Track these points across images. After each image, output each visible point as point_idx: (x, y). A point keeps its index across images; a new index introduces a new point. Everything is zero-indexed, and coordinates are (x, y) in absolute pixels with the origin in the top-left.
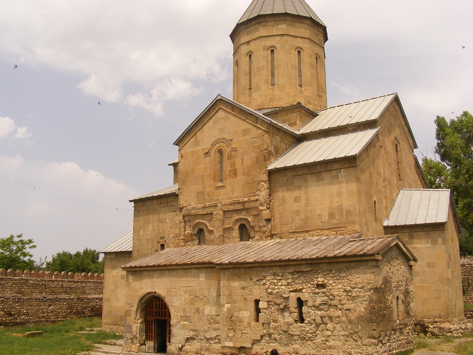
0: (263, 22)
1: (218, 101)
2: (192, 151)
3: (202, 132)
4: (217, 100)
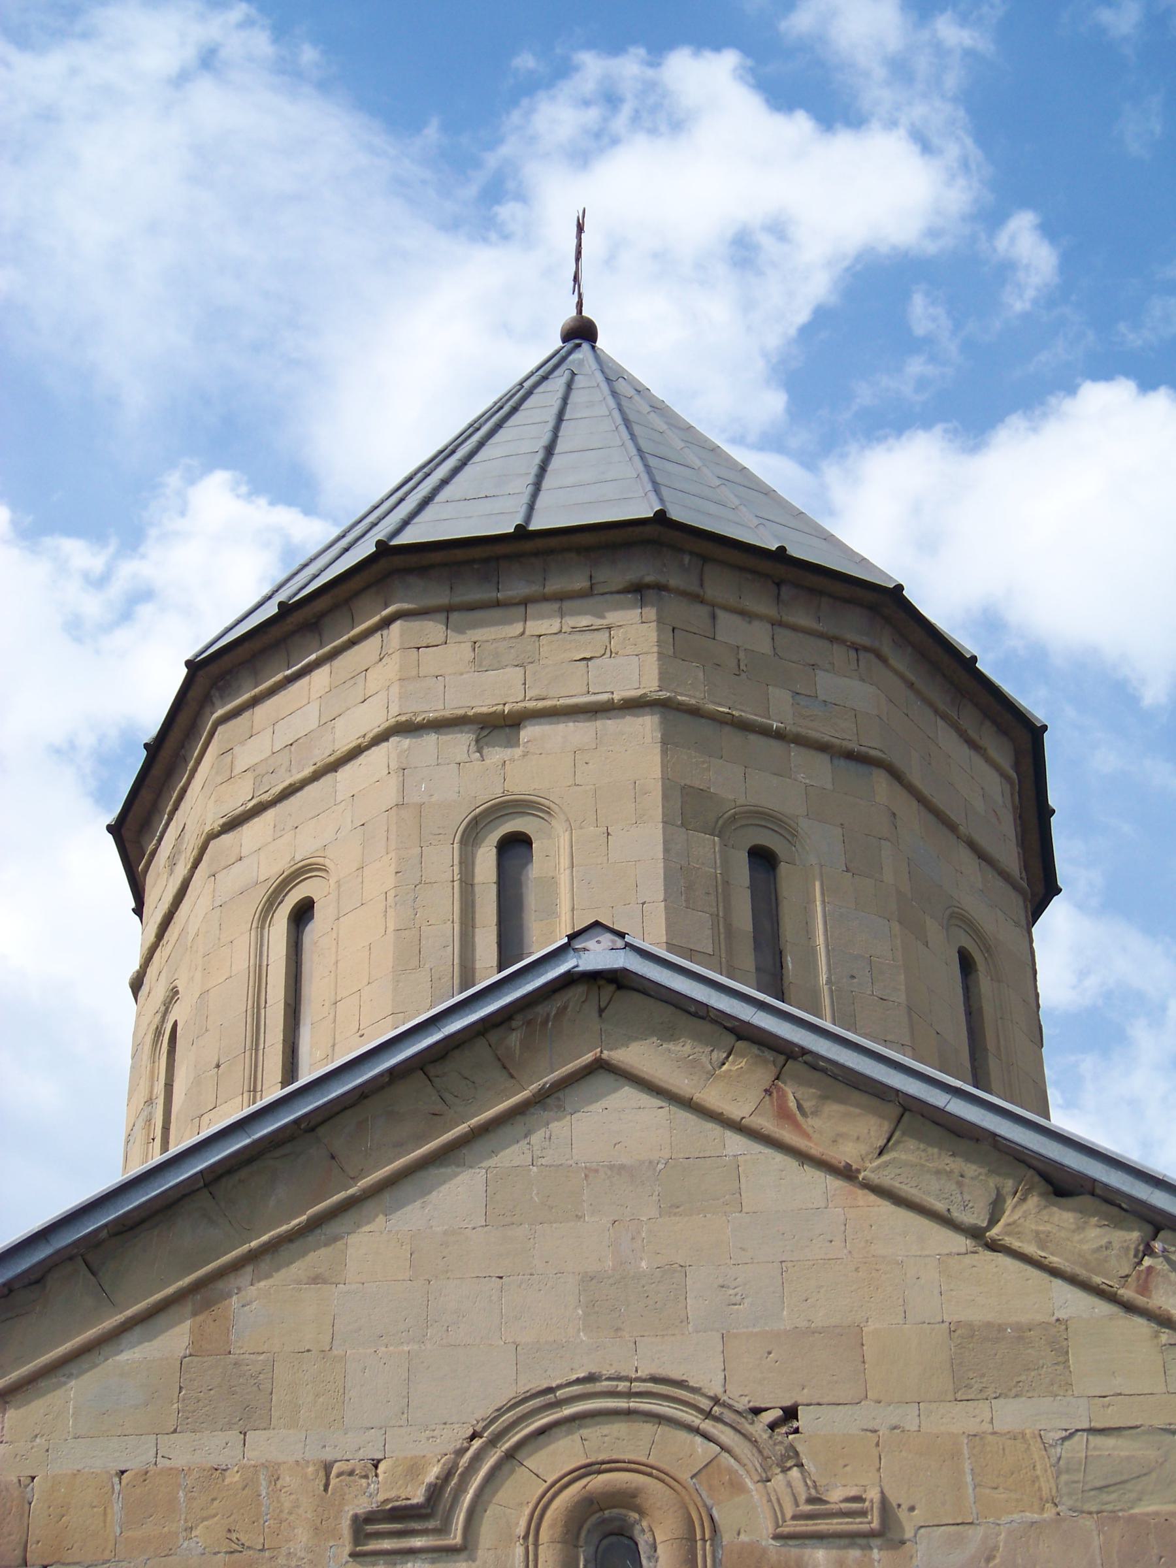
0: (683, 594)
1: (576, 993)
2: (134, 1464)
3: (316, 1280)
4: (570, 979)
